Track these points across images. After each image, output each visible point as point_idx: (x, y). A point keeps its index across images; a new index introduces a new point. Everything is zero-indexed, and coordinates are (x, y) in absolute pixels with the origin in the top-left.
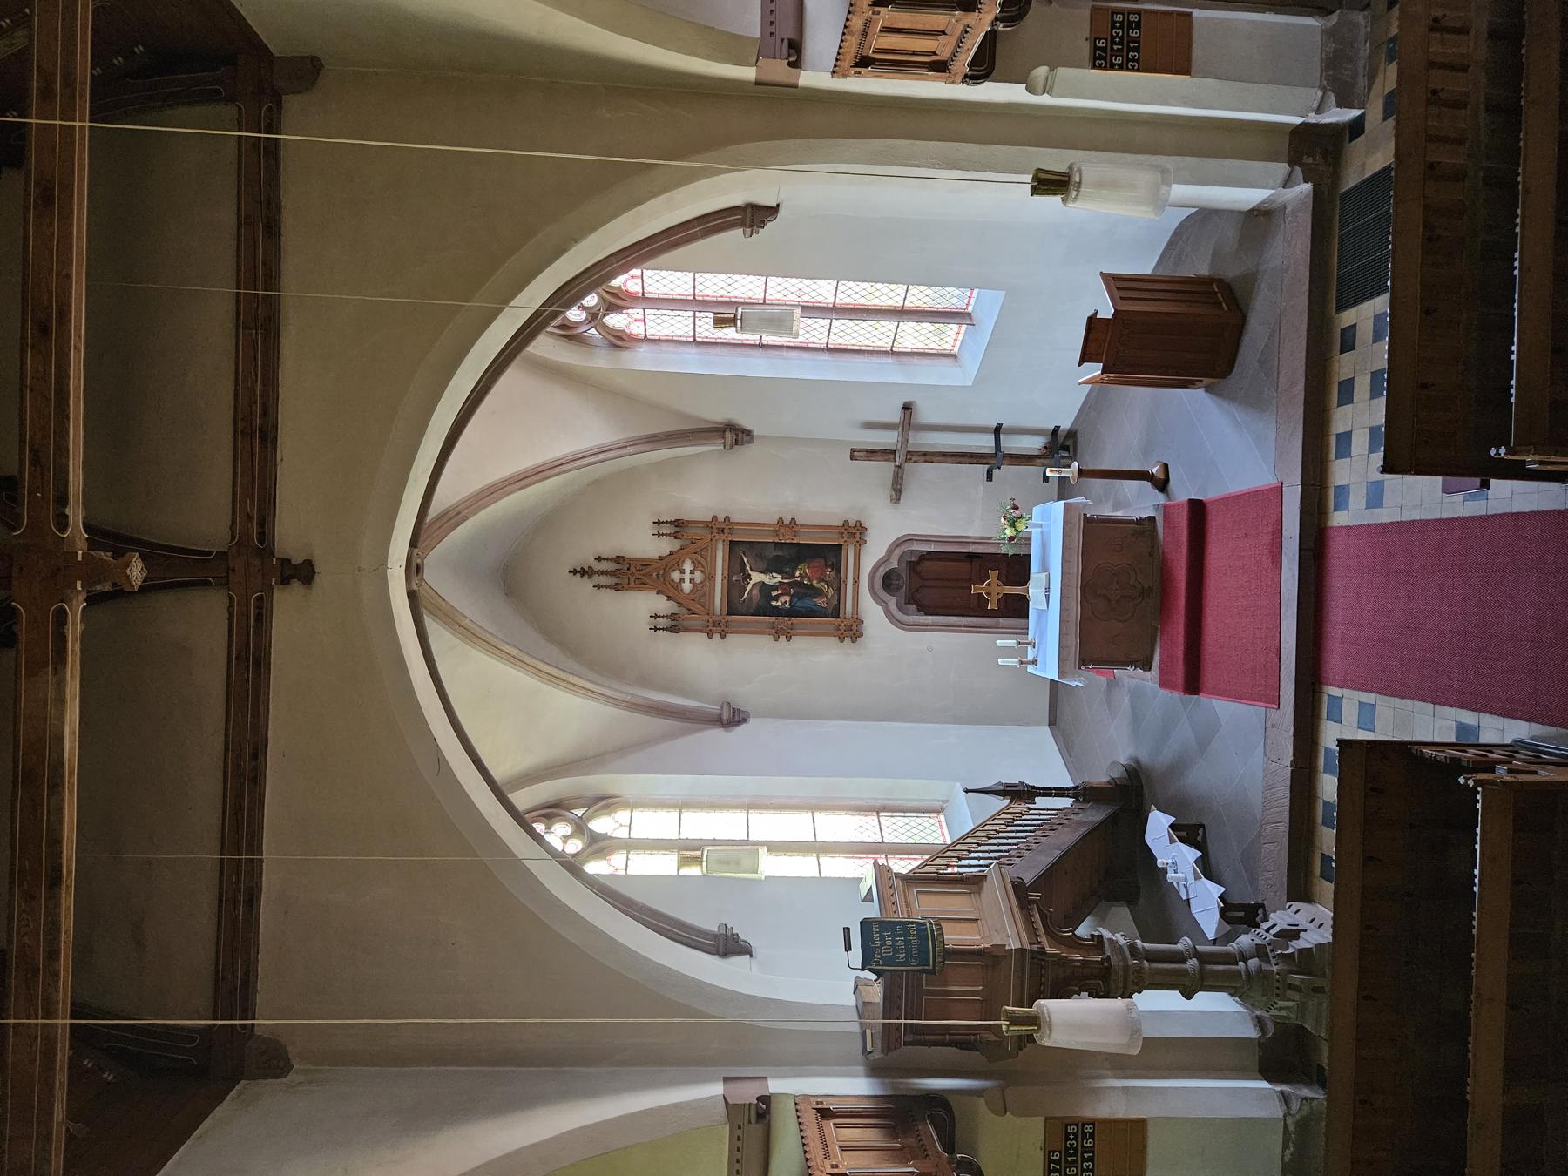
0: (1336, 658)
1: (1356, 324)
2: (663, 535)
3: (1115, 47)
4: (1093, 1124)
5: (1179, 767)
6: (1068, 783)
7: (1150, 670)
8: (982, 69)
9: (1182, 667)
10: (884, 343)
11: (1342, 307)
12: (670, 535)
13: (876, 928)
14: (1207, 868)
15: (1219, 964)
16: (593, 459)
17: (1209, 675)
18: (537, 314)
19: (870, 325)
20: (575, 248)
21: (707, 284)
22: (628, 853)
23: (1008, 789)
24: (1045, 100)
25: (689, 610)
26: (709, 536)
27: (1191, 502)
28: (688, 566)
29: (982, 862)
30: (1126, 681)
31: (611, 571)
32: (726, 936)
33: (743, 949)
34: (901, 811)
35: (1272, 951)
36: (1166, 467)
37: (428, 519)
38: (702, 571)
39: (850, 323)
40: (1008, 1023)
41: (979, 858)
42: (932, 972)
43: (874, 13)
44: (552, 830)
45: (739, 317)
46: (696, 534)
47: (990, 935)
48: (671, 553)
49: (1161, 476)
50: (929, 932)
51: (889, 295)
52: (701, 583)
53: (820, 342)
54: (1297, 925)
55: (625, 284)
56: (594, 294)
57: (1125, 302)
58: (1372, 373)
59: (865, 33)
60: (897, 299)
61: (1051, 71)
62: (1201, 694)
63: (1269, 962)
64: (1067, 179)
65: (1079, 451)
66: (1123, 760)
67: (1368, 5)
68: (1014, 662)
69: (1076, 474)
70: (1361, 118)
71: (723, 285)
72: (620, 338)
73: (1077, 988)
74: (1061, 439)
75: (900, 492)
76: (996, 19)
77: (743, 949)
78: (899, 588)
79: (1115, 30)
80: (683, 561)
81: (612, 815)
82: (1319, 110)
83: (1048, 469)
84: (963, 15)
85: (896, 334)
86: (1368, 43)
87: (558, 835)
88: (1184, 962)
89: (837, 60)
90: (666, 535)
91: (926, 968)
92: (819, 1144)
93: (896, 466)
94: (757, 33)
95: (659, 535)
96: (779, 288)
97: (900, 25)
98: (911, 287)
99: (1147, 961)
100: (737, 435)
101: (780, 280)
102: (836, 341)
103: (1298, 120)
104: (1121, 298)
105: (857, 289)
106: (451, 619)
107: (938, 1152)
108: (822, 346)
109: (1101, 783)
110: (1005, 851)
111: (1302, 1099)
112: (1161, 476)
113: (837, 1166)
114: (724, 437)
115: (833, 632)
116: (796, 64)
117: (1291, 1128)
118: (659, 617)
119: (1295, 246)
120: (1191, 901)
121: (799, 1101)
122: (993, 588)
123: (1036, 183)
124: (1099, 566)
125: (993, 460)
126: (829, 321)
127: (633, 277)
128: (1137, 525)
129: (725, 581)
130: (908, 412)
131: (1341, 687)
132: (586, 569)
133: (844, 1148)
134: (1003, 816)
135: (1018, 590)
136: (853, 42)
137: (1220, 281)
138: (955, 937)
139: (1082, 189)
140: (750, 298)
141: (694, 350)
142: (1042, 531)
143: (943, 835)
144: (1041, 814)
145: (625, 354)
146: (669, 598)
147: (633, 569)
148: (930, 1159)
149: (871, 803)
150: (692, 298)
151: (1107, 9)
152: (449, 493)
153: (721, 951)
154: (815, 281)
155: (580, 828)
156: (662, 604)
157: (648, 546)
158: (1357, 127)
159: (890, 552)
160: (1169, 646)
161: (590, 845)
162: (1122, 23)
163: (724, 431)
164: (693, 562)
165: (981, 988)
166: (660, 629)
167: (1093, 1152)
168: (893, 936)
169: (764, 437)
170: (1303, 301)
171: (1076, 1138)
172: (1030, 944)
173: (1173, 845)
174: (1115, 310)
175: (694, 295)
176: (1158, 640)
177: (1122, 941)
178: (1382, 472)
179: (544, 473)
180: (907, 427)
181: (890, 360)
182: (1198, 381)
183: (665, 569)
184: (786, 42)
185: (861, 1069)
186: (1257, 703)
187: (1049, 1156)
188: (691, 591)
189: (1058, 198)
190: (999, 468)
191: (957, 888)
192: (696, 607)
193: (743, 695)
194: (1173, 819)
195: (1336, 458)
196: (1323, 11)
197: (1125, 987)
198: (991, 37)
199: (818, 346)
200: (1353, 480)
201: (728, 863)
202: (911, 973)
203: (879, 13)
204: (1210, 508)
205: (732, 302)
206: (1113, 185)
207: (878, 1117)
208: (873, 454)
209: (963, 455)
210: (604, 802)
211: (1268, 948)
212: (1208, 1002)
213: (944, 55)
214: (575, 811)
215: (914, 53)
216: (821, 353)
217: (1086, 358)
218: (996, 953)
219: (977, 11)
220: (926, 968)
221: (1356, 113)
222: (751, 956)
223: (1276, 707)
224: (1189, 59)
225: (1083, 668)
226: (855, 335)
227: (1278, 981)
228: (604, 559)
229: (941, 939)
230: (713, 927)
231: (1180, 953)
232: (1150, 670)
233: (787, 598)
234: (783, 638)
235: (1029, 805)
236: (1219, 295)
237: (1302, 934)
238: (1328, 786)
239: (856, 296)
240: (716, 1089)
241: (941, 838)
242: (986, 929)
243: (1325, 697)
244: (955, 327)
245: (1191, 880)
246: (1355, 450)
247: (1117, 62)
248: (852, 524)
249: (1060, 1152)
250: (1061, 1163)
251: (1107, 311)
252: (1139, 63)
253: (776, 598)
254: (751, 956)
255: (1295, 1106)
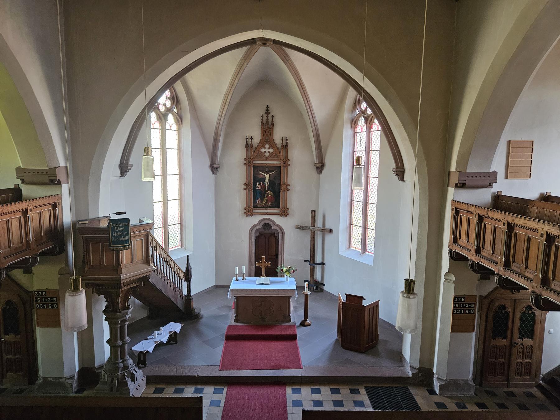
0: (238, 391)
1: (360, 394)
2: (282, 141)
3: (462, 305)
4: (57, 308)
5: (199, 333)
6: (193, 293)
7: (235, 322)
8: (455, 256)
9: (235, 333)
10: (354, 222)
11: (367, 389)
12: (282, 143)
13: (126, 224)
14: (159, 345)
15: (121, 353)
16: (310, 113)
17: (232, 344)
18: (361, 87)
19: (360, 216)
20: (387, 103)
21: (375, 155)
22: (160, 129)
23: (189, 272)
24: (443, 280)
25: (254, 151)
26: (282, 158)
27: (296, 335)
28: (271, 150)
29: (159, 263)
30: (231, 313)
31: (268, 121)
32: (128, 167)
33: (123, 174)
34: (181, 232)
35: (126, 372)
36: (309, 325)
37: (284, 48)
38: (269, 156)
39: (361, 209)
40: (75, 278)
41: (160, 262)
42: (110, 246)
43: (475, 215)
44: (168, 100)
45: (360, 166)
46: (283, 154)
47: (126, 268)
48: (275, 144)
49: (306, 324)
50: (126, 245)
51: (372, 223)
52: (265, 156)
53: (354, 198)
54: (137, 380)
55: (375, 124)
56: (371, 112)
57: (368, 310)
58: (342, 401)
59: (468, 212)
60: (370, 226)
61: (453, 281)
62: (225, 341)
63: (122, 371)
64: (411, 293)
65: (315, 293)
66: (202, 313)
67: (476, 395)
68: (237, 272)
69: (306, 293)
70: (436, 394)
71: (375, 161)
72: (355, 123)
73: (108, 300)
74: (320, 286)
75: (300, 229)
76: (473, 261)
77: (123, 174)
78: (265, 230)
79: (468, 304)
80: (273, 149)
81: (175, 123)
82: (438, 379)
83: (308, 283)
84: (474, 249)
85: (357, 226)
86: (463, 396)
87: (164, 100)
88: (121, 340)
89: (458, 202)
90: (282, 142)
91: (111, 244)
92: (40, 204)
93: (309, 227)
94: (469, 171)
95: (282, 139)
96: (374, 183)
97: (471, 225)
98: (374, 231)
99: (120, 326)
100: (320, 168)
101: (377, 183)
102: (355, 204)
103: (435, 371)
104: (370, 308)
105: (374, 211)
106: (247, 57)
107: (40, 250)
108: (353, 199)
109: (193, 305)
110: (163, 271)
111: (72, 384)
112: (306, 324)
113: (31, 211)
114: (319, 163)
115: (248, 205)
116: (456, 186)
117: (61, 380)
118: (251, 140)
119: (389, 371)
120: (147, 340)
121: (60, 196)
122: (264, 264)
123: (409, 281)
124: (273, 303)
125: (312, 262)
126: (362, 201)
127: (378, 127)
128: (288, 316)
129: (265, 165)
130: (329, 231)
131: (227, 393)
132: (269, 112)
133: (40, 213)
134: (178, 270)
135: (263, 273)
136: (465, 208)
137: (376, 343)
138: (125, 255)
139: (407, 299)
140: (370, 172)
141: (351, 151)
142: (285, 281)
143: (175, 247)
144: (180, 284)
145: (349, 125)
146: (259, 144)
147: (269, 129)
148: (37, 247)
149: (184, 221)
150: (370, 150)
151: (476, 301)
152: (296, 57)
153: (121, 165)
154: (377, 196)
155: (169, 110)
156: (256, 140)
157: (278, 135)
158: (432, 392)
159: (278, 226)
160: (243, 329)
161: (162, 114)
162: (470, 307)
163: (321, 163)
164: (273, 152)
165: (105, 265)
166: (247, 140)
167: (46, 308)
168: (123, 231)
169: (320, 177)
170: (369, 375)
171: (51, 301)
172: (123, 283)
173: (168, 333)
174: (365, 306)
175: (371, 151)
176: (246, 325)
177: (128, 317)
178: (302, 410)
179: (304, 94)
180: (323, 231)
181: (348, 224)
182: (340, 337)
183: (269, 142)
184: (465, 182)
185: (74, 219)
186: (221, 362)
187: (43, 292)
188: (261, 152)
189: (404, 289)
190: (309, 265)
191: (145, 255)
192: (256, 153)
193: (223, 173)
194: (178, 333)
195: (311, 388)
196: (474, 380)
197: (110, 319)
198: (466, 259)
199: (353, 197)
200: (303, 395)
201: (148, 166)
202: (109, 238)
203: (475, 217)
204: (294, 342)
205: (369, 165)
206: (409, 311)
207: (54, 226)
208: (313, 218)
209: (314, 252)
210: (179, 120)
211: (127, 370)
212: (107, 348)
213: (460, 242)
214: (176, 108)
215: (460, 231)
216: (350, 199)
217: (211, 405)
218: (119, 270)
219: (476, 254)
220: (111, 244)
221: (437, 392)
222: (120, 177)
223: (220, 369)
224: (457, 331)
225: (235, 297)
226: (357, 211)
227: (115, 374)
228: (273, 118)
229: (123, 249)
230: (131, 162)
231: (124, 338)
232: (235, 322)
233: (260, 188)
234: (245, 187)
235: (183, 279)
236: (371, 343)
237: (133, 382)
238: (189, 392)
239: (371, 211)
240: (62, 164)
241: (171, 247)
242: (129, 266)
243: (223, 387)
244: (360, 247)
245: (155, 340)
246: (314, 395)
247: (456, 305)
248: (288, 211)
249: (46, 296)
250: (42, 296)
251: (365, 303)
252: (456, 313)
253: (260, 184)
254: (120, 177)
255: (69, 381)
